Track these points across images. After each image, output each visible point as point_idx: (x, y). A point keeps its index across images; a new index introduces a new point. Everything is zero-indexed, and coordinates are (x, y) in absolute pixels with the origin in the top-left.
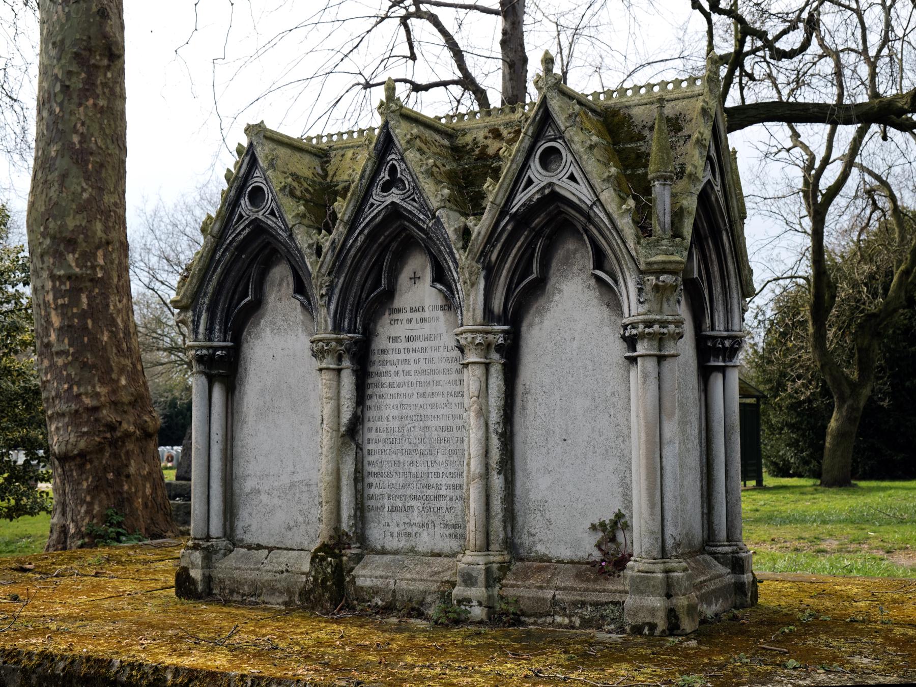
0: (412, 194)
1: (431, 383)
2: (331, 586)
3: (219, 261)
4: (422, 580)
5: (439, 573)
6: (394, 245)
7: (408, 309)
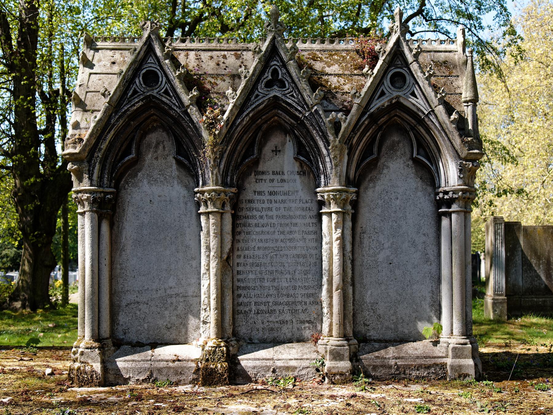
0: (292, 91)
1: (290, 225)
3: (114, 125)
7: (271, 172)
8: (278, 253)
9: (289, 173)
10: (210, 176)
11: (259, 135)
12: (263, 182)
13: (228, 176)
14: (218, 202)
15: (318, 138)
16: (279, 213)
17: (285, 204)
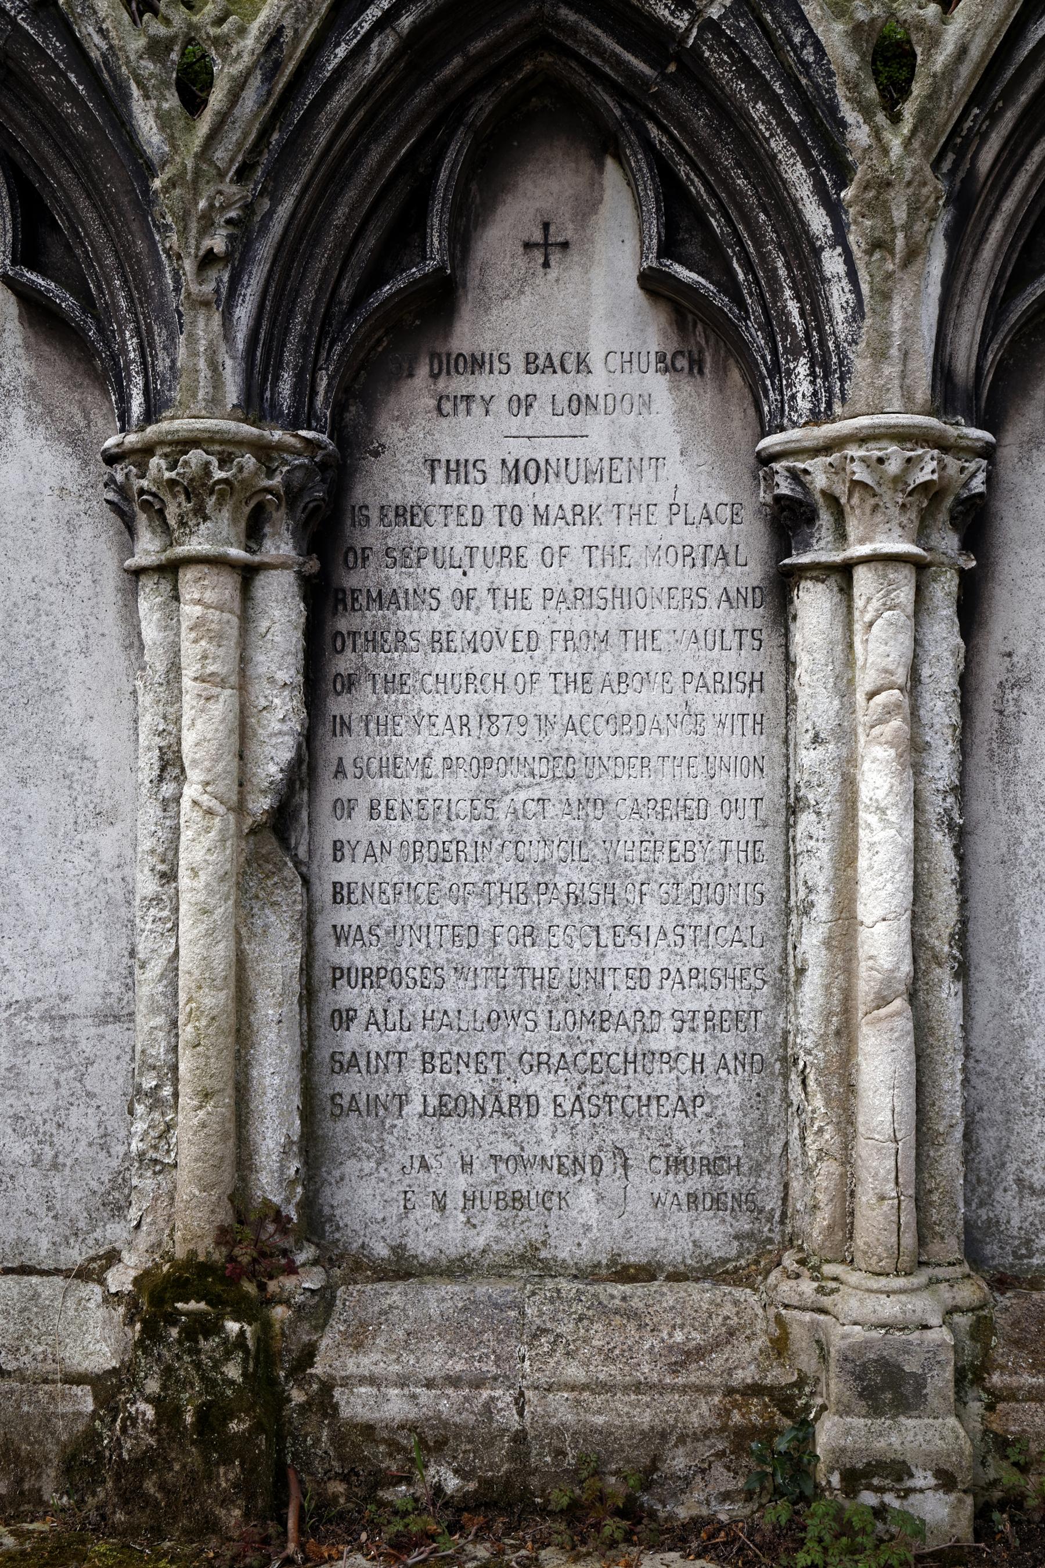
2: (247, 1438)
4: (638, 1387)
5: (700, 1353)
6: (484, 105)
7: (518, 361)
9: (614, 361)
12: (477, 408)
13: (279, 366)
15: (778, 144)
16: (557, 576)
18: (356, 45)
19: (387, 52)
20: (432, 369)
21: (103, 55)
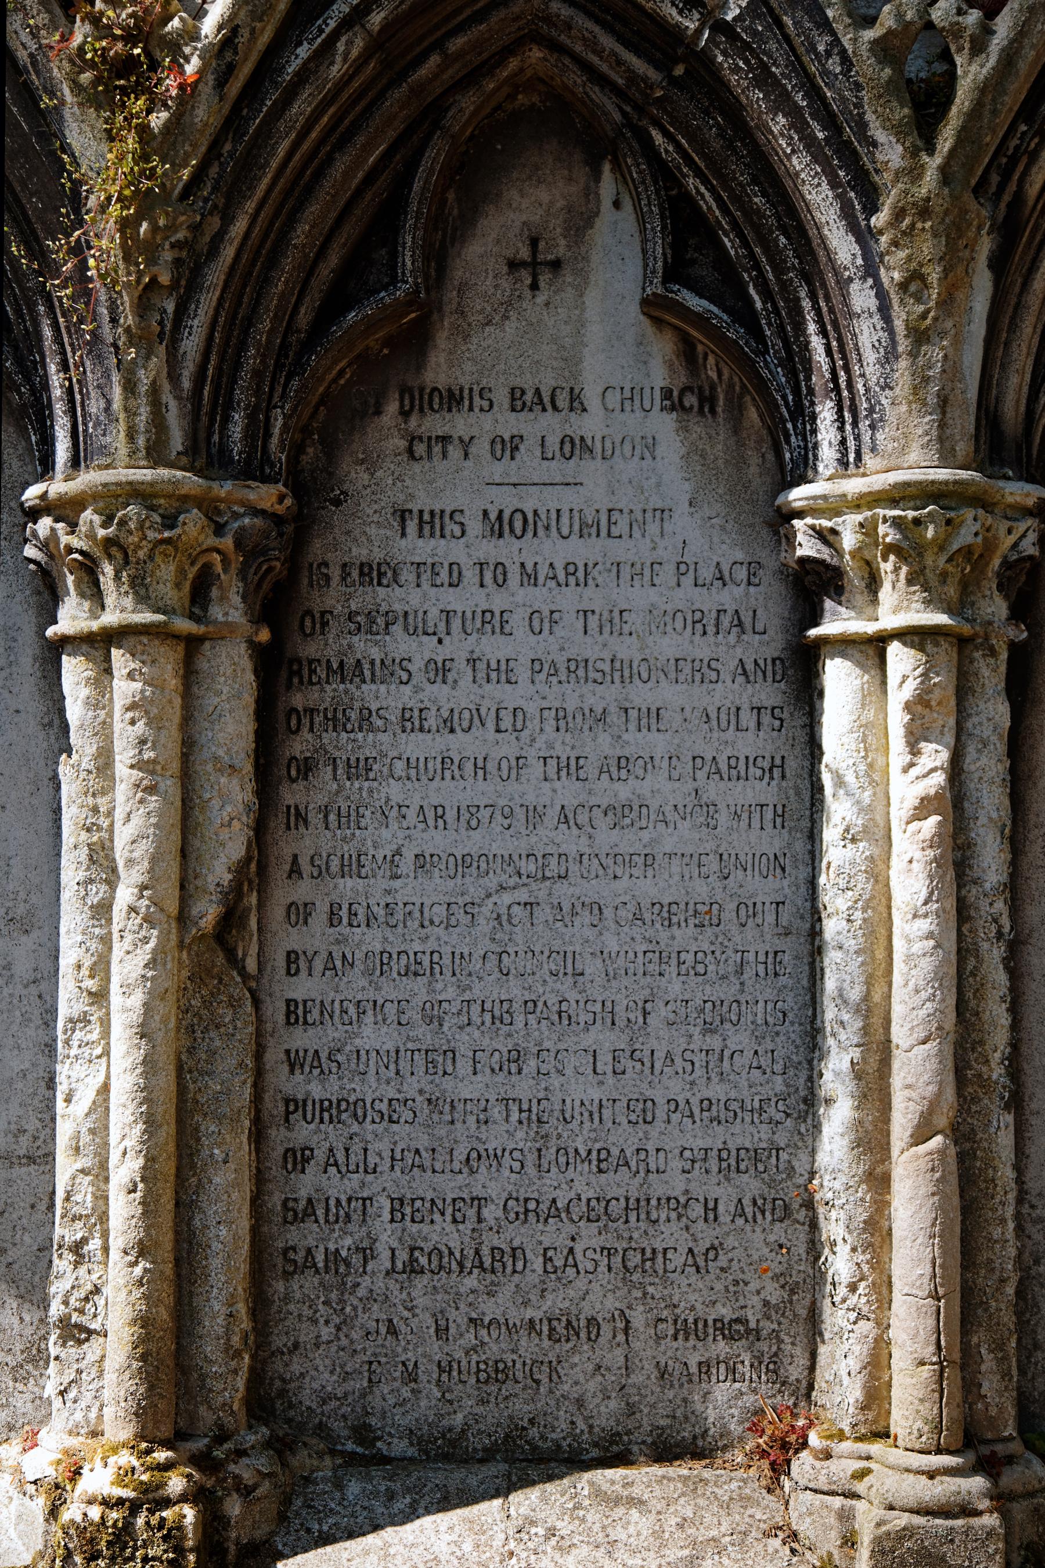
1: (615, 717)
7: (501, 396)
8: (541, 891)
9: (614, 399)
10: (117, 405)
11: (426, 163)
12: (455, 452)
13: (229, 406)
14: (167, 571)
16: (547, 646)
17: (590, 591)
18: (321, 45)
19: (355, 53)
20: (402, 406)
21: (31, 55)
